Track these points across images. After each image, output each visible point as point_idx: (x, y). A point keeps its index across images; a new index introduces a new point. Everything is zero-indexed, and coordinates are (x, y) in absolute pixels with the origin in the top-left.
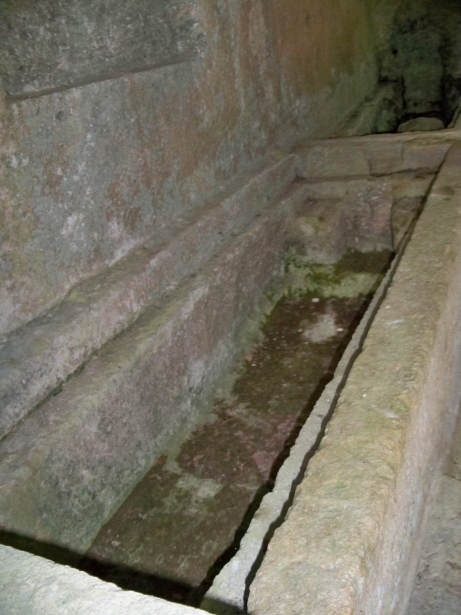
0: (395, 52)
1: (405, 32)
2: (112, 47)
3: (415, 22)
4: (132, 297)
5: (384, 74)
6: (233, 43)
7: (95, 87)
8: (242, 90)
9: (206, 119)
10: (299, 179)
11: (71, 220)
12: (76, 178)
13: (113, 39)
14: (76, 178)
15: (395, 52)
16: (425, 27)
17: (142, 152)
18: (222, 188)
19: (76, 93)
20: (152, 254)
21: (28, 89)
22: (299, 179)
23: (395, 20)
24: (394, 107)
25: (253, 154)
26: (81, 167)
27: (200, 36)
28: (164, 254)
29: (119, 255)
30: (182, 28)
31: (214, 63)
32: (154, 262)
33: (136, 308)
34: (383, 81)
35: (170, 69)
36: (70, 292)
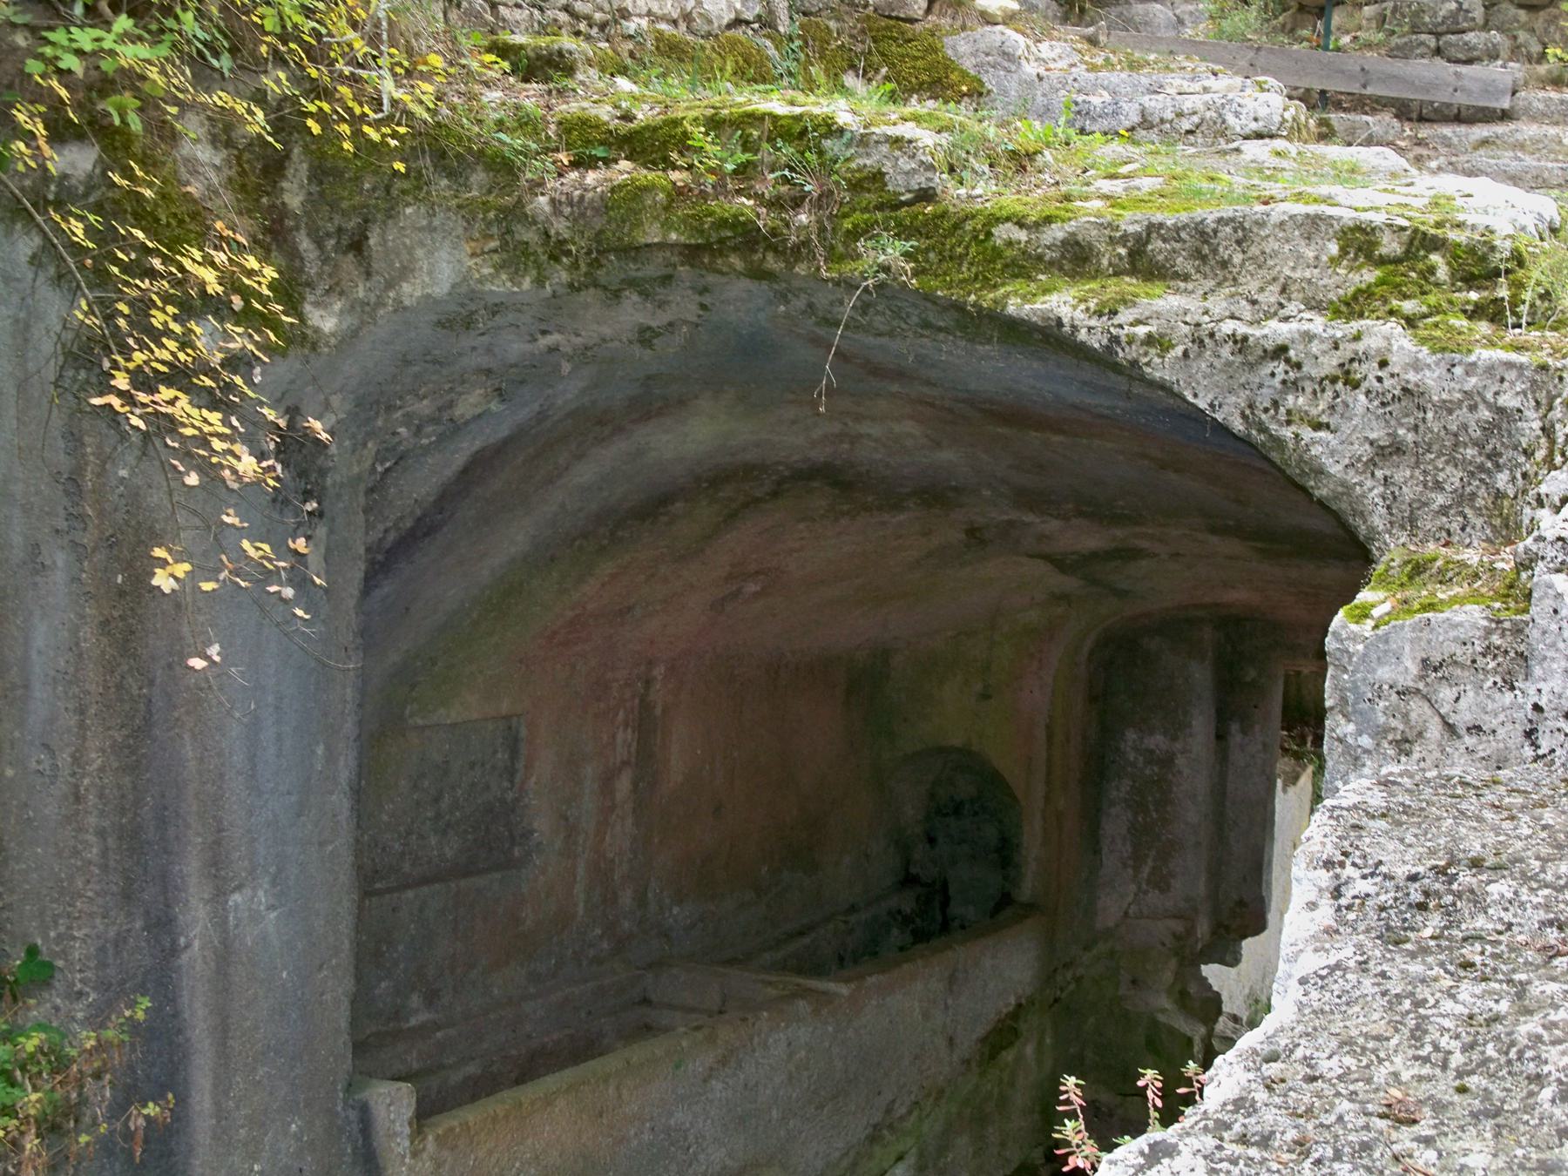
0: (932, 841)
1: (946, 815)
2: (449, 853)
3: (962, 803)
4: (414, 1055)
5: (913, 870)
6: (580, 849)
7: (425, 889)
8: (582, 896)
9: (528, 922)
10: (646, 1001)
11: (383, 985)
12: (395, 955)
13: (451, 848)
14: (395, 955)
15: (932, 841)
16: (976, 814)
17: (1451, 579)
18: (532, 990)
19: (410, 894)
20: (439, 1029)
21: (378, 886)
22: (646, 1001)
23: (932, 796)
24: (911, 927)
25: (585, 963)
26: (401, 948)
27: (540, 843)
28: (452, 1032)
29: (413, 1022)
30: (523, 836)
31: (550, 869)
32: (439, 1035)
33: (415, 1066)
34: (908, 880)
35: (497, 876)
36: (369, 1036)
